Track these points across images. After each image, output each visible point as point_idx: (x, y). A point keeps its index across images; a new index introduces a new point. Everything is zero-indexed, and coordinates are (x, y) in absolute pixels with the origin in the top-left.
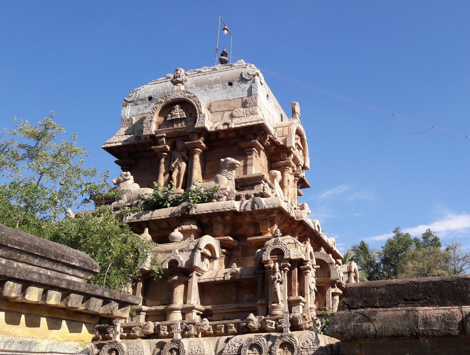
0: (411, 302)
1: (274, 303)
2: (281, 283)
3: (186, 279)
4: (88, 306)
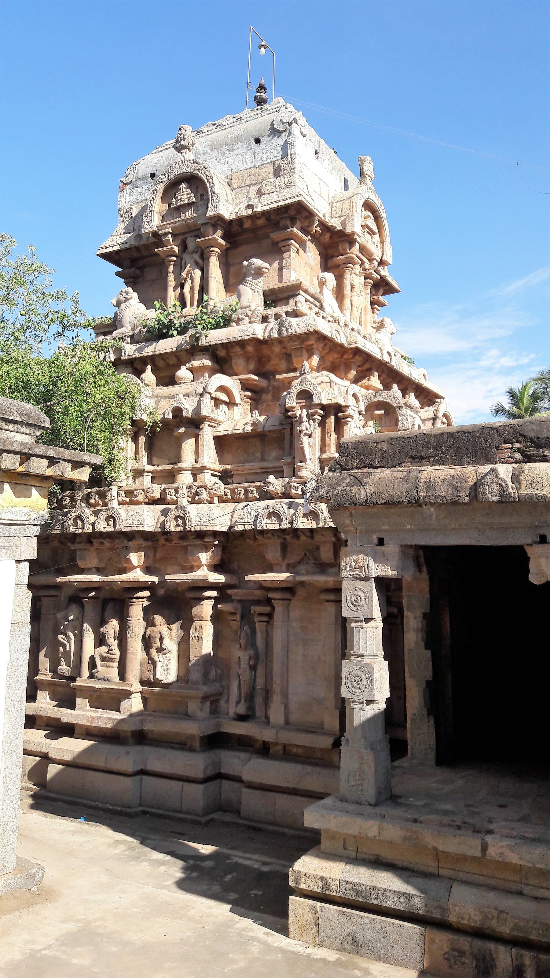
0: (418, 460)
1: (301, 462)
2: (310, 436)
3: (196, 431)
4: (28, 466)
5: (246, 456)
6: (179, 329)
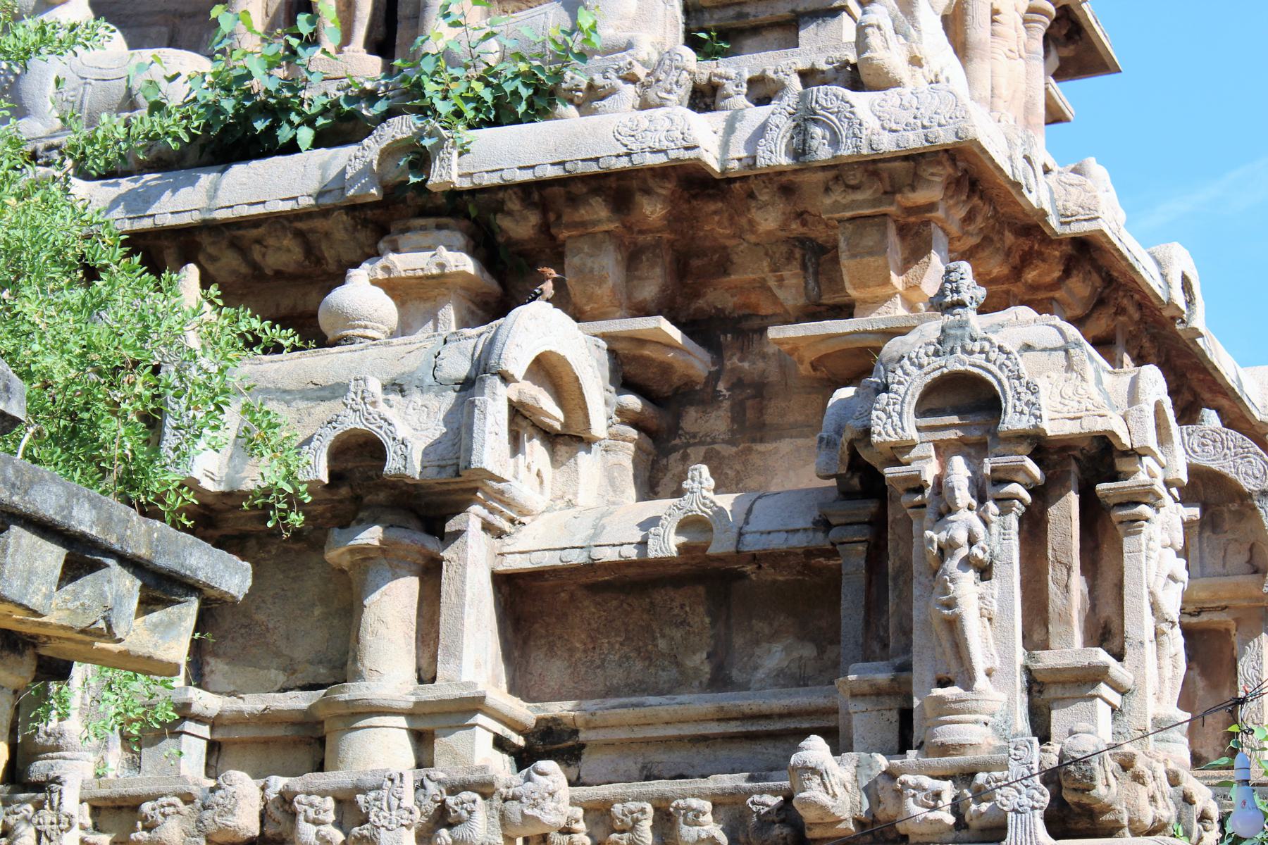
1: (943, 683)
2: (985, 572)
3: (431, 544)
5: (639, 665)
6: (320, 121)
